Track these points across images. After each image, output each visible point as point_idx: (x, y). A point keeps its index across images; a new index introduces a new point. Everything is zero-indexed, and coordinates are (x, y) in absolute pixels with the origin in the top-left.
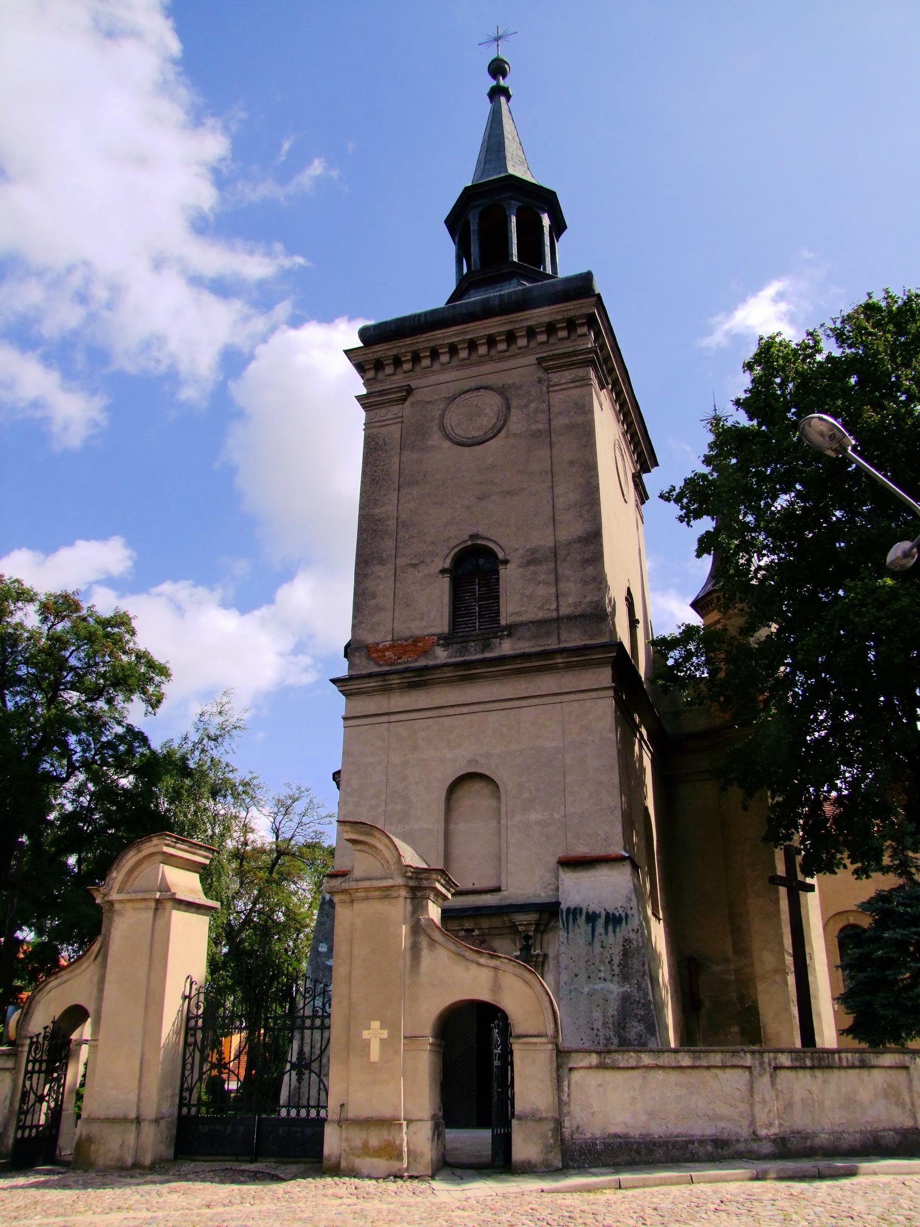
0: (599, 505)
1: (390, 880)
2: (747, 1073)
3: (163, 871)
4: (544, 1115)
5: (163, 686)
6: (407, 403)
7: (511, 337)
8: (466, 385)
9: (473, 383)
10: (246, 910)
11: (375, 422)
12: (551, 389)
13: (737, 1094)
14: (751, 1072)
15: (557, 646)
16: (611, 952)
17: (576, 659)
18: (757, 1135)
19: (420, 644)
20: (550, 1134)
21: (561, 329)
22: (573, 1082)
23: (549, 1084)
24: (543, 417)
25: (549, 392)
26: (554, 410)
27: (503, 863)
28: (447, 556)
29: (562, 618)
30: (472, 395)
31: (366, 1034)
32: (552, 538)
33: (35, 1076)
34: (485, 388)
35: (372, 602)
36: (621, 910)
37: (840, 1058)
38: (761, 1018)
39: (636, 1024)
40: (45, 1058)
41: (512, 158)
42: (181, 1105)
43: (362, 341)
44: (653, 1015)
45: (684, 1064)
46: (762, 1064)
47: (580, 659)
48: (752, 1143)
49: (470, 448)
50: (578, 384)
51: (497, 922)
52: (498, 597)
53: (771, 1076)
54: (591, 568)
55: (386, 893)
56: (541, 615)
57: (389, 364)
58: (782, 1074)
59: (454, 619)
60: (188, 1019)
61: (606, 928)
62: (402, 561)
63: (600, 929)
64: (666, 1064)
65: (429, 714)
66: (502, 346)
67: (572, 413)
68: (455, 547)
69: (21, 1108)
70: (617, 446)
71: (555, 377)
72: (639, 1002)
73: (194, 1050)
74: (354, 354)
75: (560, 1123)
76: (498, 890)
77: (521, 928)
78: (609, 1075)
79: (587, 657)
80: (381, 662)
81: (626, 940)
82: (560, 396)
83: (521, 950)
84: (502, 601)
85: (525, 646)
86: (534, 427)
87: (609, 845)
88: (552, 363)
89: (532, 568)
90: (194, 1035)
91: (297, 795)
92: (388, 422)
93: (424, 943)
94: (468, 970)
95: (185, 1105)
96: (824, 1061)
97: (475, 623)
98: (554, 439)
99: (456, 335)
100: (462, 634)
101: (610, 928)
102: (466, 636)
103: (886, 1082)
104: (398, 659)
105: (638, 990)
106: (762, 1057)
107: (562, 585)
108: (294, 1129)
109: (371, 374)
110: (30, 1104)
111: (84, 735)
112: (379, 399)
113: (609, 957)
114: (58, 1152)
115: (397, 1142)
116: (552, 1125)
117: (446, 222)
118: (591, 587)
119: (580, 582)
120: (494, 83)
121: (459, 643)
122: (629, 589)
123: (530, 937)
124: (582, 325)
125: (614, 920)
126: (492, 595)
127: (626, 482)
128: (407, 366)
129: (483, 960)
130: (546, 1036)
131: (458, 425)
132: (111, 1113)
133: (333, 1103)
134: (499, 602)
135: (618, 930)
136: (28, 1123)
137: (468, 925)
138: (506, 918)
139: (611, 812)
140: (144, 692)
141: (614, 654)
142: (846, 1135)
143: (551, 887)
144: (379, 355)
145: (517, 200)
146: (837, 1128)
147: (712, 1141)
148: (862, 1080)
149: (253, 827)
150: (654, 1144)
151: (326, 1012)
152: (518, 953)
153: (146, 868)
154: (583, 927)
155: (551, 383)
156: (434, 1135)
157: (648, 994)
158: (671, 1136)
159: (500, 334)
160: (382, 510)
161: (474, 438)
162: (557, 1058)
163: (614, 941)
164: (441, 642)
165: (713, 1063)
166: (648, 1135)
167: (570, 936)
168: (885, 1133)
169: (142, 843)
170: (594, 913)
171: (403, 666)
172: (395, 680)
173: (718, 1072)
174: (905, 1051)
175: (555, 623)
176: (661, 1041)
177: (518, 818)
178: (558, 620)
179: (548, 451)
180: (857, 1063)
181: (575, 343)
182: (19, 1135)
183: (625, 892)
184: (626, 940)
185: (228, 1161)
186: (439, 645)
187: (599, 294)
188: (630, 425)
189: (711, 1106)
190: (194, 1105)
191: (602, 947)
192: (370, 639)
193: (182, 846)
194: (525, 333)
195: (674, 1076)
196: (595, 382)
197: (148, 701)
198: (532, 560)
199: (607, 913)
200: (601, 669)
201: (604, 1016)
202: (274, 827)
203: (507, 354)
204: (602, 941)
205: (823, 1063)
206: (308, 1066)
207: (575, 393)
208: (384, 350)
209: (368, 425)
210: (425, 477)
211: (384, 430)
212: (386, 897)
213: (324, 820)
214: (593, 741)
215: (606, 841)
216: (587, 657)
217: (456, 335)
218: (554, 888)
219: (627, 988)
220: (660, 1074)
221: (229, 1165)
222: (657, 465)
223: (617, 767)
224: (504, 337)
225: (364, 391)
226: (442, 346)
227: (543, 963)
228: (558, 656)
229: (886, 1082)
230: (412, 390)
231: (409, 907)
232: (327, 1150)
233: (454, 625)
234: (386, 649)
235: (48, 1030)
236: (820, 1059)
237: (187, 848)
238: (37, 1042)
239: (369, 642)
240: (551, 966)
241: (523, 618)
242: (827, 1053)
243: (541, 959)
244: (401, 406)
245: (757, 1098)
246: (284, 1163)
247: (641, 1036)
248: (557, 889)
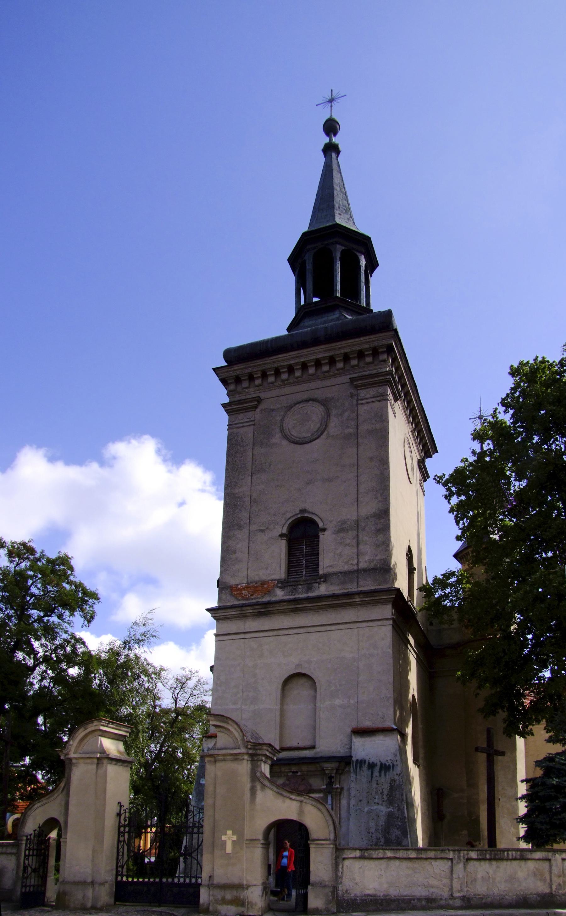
0: (389, 490)
1: (238, 750)
2: (450, 862)
3: (101, 741)
4: (327, 883)
5: (95, 606)
6: (258, 410)
7: (332, 361)
8: (300, 397)
9: (304, 396)
10: (156, 750)
11: (236, 424)
12: (359, 402)
13: (443, 873)
14: (452, 862)
15: (356, 590)
16: (383, 787)
18: (453, 896)
19: (265, 586)
20: (330, 894)
21: (368, 355)
22: (345, 866)
23: (330, 867)
24: (353, 423)
25: (357, 404)
26: (361, 418)
27: (317, 730)
28: (284, 525)
29: (360, 570)
31: (224, 838)
32: (356, 514)
33: (30, 858)
34: (313, 400)
35: (234, 556)
36: (390, 762)
37: (508, 854)
38: (481, 826)
39: (395, 830)
40: (35, 847)
41: (339, 208)
42: (117, 875)
43: (226, 361)
44: (406, 825)
45: (411, 856)
47: (371, 599)
48: (449, 901)
49: (301, 446)
50: (379, 398)
51: (312, 768)
52: (318, 554)
53: (464, 864)
54: (381, 536)
55: (236, 758)
56: (346, 568)
57: (245, 380)
58: (471, 863)
59: (288, 569)
60: (120, 827)
62: (254, 527)
63: (376, 773)
64: (401, 856)
65: (271, 633)
66: (326, 368)
67: (373, 421)
68: (289, 519)
69: (23, 875)
70: (406, 442)
71: (363, 393)
72: (398, 818)
73: (123, 844)
74: (221, 372)
75: (336, 888)
76: (313, 747)
77: (327, 772)
78: (367, 863)
79: (376, 598)
80: (240, 598)
81: (392, 780)
82: (366, 407)
83: (326, 785)
84: (321, 558)
85: (335, 589)
86: (347, 431)
87: (385, 721)
88: (360, 382)
89: (342, 535)
90: (124, 836)
91: (190, 676)
92: (245, 424)
93: (258, 787)
94: (284, 802)
95: (120, 875)
96: (498, 855)
97: (303, 572)
98: (360, 440)
100: (294, 579)
101: (383, 772)
102: (296, 581)
103: (535, 868)
104: (251, 595)
105: (398, 810)
106: (460, 853)
107: (361, 547)
109: (232, 387)
110: (29, 873)
111: (43, 641)
112: (238, 407)
113: (381, 790)
114: (46, 900)
115: (241, 897)
116: (331, 889)
117: (288, 260)
118: (381, 549)
119: (374, 546)
120: (327, 140)
121: (291, 586)
122: (409, 547)
123: (333, 777)
124: (383, 352)
125: (385, 768)
126: (314, 553)
127: (413, 469)
128: (258, 382)
129: (293, 797)
130: (330, 840)
132: (77, 879)
133: (205, 875)
134: (319, 558)
135: (387, 774)
136: (28, 884)
137: (294, 769)
138: (318, 766)
140: (83, 610)
141: (394, 596)
142: (507, 897)
143: (347, 746)
144: (238, 372)
145: (342, 245)
146: (502, 893)
147: (425, 899)
148: (521, 867)
149: (160, 696)
150: (391, 900)
151: (201, 824)
152: (325, 787)
153: (90, 739)
154: (365, 772)
155: (359, 398)
156: (263, 893)
157: (404, 813)
158: (402, 896)
159: (324, 358)
160: (241, 490)
161: (304, 438)
162: (336, 852)
163: (385, 781)
164: (279, 585)
165: (429, 856)
166: (388, 895)
167: (358, 777)
168: (531, 896)
169: (87, 723)
170: (373, 763)
171: (254, 601)
172: (249, 611)
173: (433, 862)
174: (549, 851)
175: (357, 573)
176: (411, 841)
177: (327, 703)
178: (358, 571)
179: (355, 449)
180: (518, 857)
181: (377, 367)
182: (23, 890)
183: (393, 751)
184: (392, 780)
185: (146, 906)
186: (278, 587)
188: (417, 425)
189: (426, 880)
193: (112, 726)
194: (342, 358)
195: (405, 864)
196: (391, 397)
197: (85, 617)
198: (342, 529)
199: (381, 764)
200: (385, 606)
201: (377, 825)
202: (174, 696)
203: (329, 374)
204: (377, 781)
205: (497, 857)
206: (190, 855)
207: (377, 405)
208: (242, 369)
209: (230, 426)
210: (270, 466)
211: (242, 431)
212: (236, 760)
213: (208, 693)
215: (383, 718)
216: (376, 598)
217: (293, 358)
218: (349, 747)
219: (391, 809)
220: (397, 863)
221: (146, 908)
222: (437, 452)
223: (392, 671)
224: (327, 361)
225: (227, 400)
226: (283, 367)
227: (340, 793)
228: (357, 596)
229: (535, 868)
230: (262, 400)
231: (249, 766)
232: (201, 901)
233: (288, 573)
234: (243, 589)
235: (36, 832)
236: (495, 855)
237: (115, 727)
238: (30, 839)
239: (231, 584)
240: (345, 794)
241: (335, 570)
242: (500, 851)
243: (339, 790)
244: (253, 412)
245: (455, 876)
246: (177, 907)
247: (398, 838)
248: (351, 748)
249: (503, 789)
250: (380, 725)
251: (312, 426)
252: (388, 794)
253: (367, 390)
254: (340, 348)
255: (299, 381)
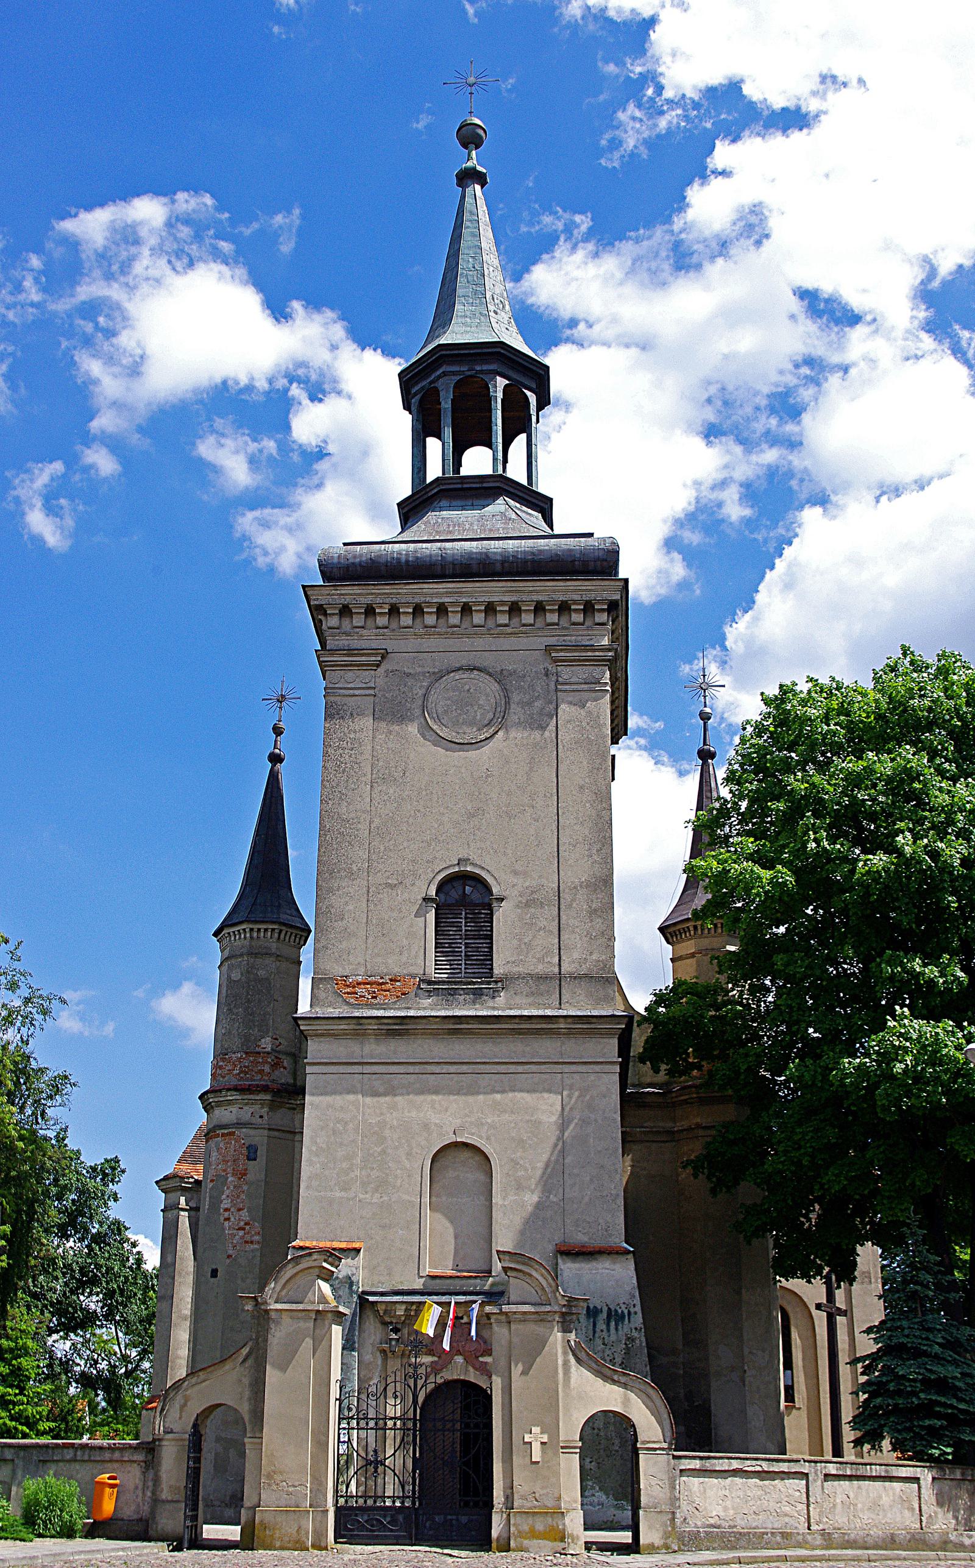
6: (381, 670)
7: (515, 609)
9: (464, 660)
11: (341, 688)
17: (580, 1026)
30: (463, 676)
36: (623, 1307)
46: (816, 1473)
61: (608, 1325)
63: (601, 1325)
65: (411, 1069)
66: (503, 619)
71: (566, 673)
79: (593, 1026)
87: (611, 1235)
92: (357, 692)
99: (448, 594)
108: (449, 1517)
128: (382, 621)
131: (446, 712)
139: (613, 1200)
153: (300, 1280)
159: (503, 603)
187: (626, 581)
190: (370, 1497)
191: (604, 1344)
192: (338, 970)
203: (508, 630)
214: (596, 1120)
216: (593, 1026)
217: (448, 594)
226: (430, 604)
241: (520, 969)
249: (750, 1353)
250: (599, 1242)
251: (478, 714)
252: (623, 1363)
253: (573, 668)
254: (531, 592)
255: (453, 632)
